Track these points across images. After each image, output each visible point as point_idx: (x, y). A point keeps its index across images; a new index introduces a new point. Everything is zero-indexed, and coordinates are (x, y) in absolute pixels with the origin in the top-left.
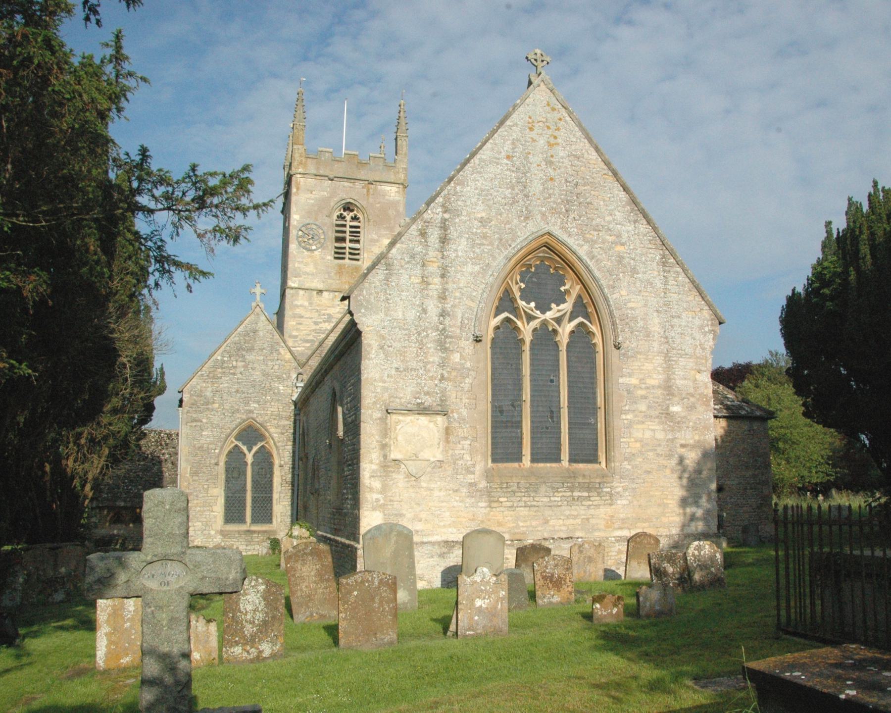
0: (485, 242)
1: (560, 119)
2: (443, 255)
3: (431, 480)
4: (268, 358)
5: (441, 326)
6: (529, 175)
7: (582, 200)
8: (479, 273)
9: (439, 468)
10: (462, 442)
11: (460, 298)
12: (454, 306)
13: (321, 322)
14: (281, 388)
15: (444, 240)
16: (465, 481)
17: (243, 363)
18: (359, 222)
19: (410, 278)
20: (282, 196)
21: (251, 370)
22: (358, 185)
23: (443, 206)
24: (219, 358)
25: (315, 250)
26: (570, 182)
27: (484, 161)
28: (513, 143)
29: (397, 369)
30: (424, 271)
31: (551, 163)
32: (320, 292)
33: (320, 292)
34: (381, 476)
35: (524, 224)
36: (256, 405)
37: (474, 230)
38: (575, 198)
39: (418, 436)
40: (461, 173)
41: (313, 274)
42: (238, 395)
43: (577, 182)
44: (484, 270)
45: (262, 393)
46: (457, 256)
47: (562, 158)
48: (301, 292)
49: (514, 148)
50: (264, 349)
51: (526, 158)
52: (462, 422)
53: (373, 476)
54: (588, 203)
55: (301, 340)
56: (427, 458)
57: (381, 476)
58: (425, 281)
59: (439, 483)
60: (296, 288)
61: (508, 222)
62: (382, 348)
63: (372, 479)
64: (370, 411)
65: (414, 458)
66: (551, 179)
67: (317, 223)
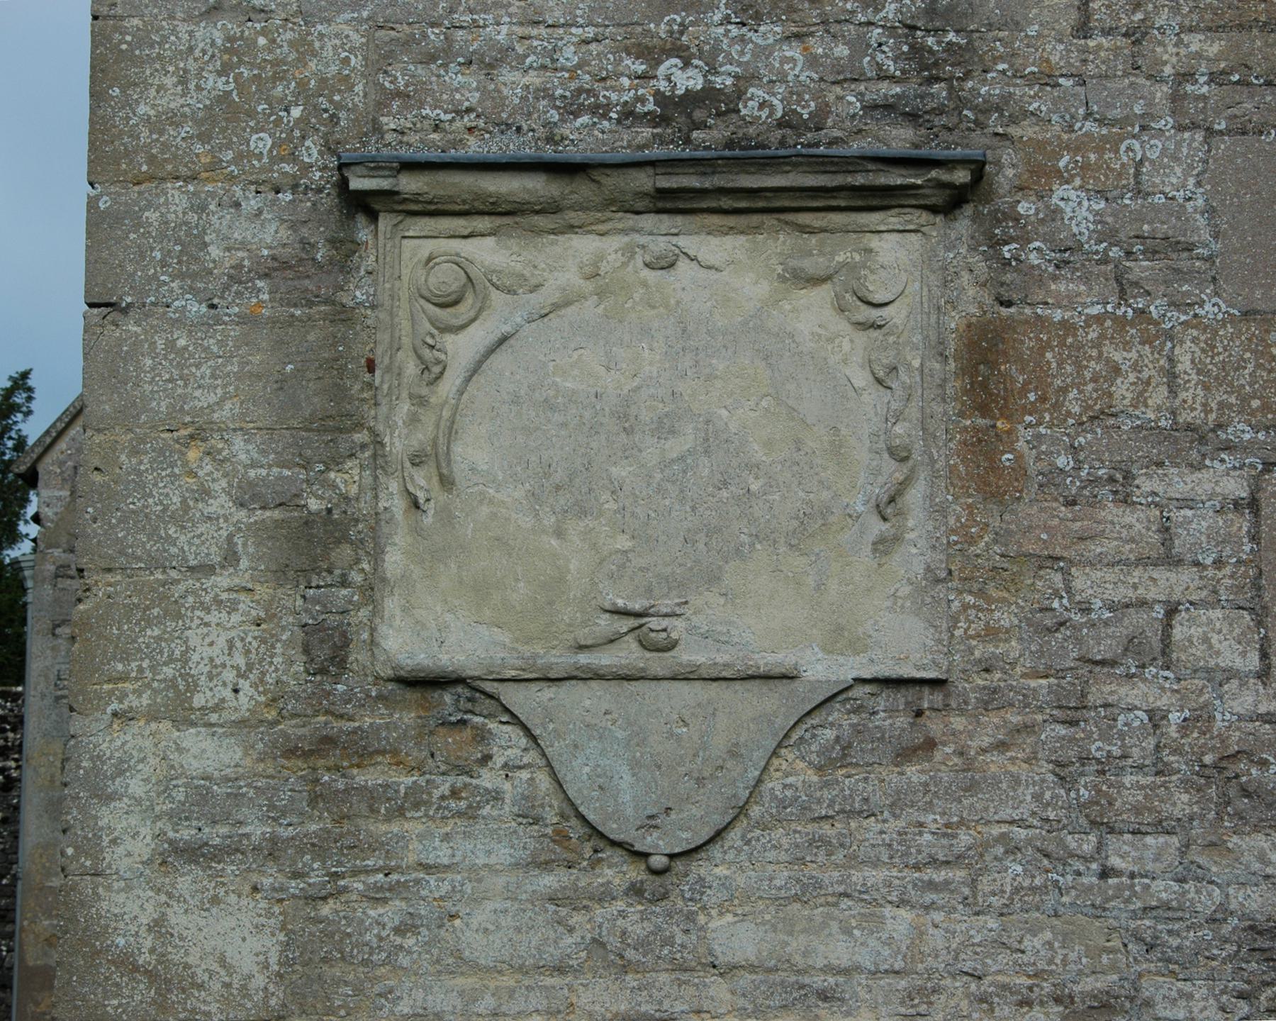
3: (806, 893)
9: (905, 755)
10: (1146, 484)
16: (1206, 900)
34: (272, 850)
39: (665, 428)
52: (1141, 268)
53: (193, 853)
56: (766, 660)
57: (272, 850)
59: (900, 921)
63: (187, 881)
64: (176, 198)
65: (628, 655)
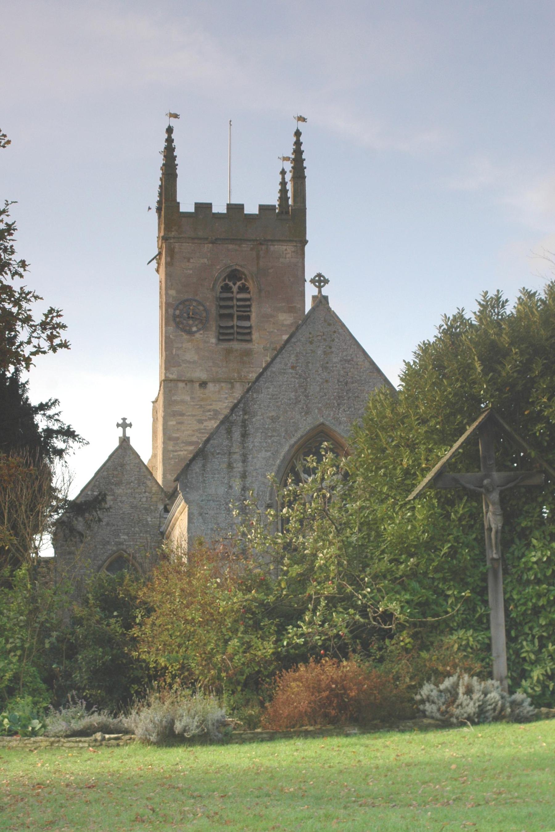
0: (274, 433)
1: (335, 332)
2: (244, 446)
4: (136, 491)
5: (243, 498)
6: (308, 380)
7: (350, 395)
8: (270, 457)
11: (256, 477)
12: (252, 482)
13: (206, 420)
14: (149, 519)
15: (244, 435)
17: (112, 497)
18: (249, 293)
19: (220, 465)
20: (155, 261)
21: (119, 504)
22: (246, 247)
23: (243, 410)
24: (89, 493)
25: (196, 332)
26: (341, 382)
27: (274, 372)
28: (297, 356)
29: (212, 529)
30: (230, 458)
31: (326, 368)
32: (203, 384)
33: (203, 384)
35: (304, 418)
36: (126, 537)
37: (267, 426)
38: (345, 394)
40: (257, 383)
41: (194, 362)
42: (109, 528)
43: (347, 381)
44: (274, 455)
45: (131, 526)
46: (254, 446)
47: (336, 363)
48: (181, 385)
49: (297, 360)
50: (132, 482)
51: (307, 366)
54: (355, 397)
55: (183, 442)
58: (230, 466)
60: (175, 380)
61: (292, 418)
62: (201, 514)
66: (327, 381)
67: (197, 298)
